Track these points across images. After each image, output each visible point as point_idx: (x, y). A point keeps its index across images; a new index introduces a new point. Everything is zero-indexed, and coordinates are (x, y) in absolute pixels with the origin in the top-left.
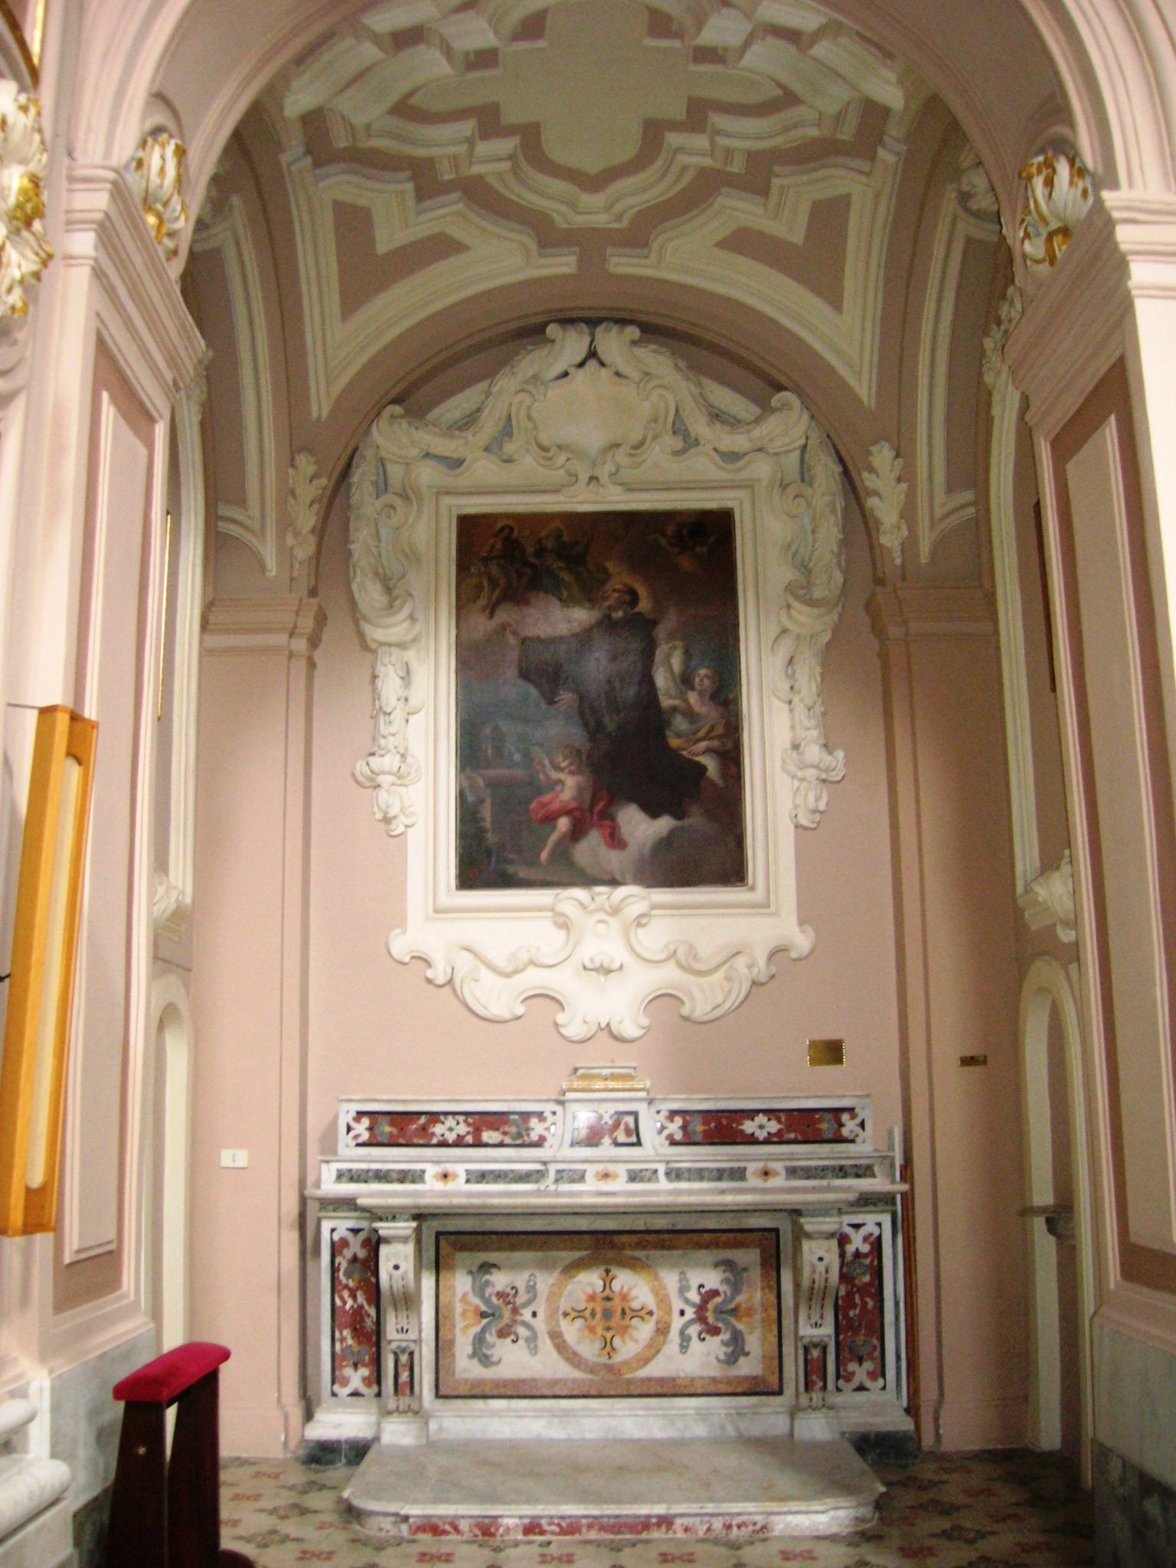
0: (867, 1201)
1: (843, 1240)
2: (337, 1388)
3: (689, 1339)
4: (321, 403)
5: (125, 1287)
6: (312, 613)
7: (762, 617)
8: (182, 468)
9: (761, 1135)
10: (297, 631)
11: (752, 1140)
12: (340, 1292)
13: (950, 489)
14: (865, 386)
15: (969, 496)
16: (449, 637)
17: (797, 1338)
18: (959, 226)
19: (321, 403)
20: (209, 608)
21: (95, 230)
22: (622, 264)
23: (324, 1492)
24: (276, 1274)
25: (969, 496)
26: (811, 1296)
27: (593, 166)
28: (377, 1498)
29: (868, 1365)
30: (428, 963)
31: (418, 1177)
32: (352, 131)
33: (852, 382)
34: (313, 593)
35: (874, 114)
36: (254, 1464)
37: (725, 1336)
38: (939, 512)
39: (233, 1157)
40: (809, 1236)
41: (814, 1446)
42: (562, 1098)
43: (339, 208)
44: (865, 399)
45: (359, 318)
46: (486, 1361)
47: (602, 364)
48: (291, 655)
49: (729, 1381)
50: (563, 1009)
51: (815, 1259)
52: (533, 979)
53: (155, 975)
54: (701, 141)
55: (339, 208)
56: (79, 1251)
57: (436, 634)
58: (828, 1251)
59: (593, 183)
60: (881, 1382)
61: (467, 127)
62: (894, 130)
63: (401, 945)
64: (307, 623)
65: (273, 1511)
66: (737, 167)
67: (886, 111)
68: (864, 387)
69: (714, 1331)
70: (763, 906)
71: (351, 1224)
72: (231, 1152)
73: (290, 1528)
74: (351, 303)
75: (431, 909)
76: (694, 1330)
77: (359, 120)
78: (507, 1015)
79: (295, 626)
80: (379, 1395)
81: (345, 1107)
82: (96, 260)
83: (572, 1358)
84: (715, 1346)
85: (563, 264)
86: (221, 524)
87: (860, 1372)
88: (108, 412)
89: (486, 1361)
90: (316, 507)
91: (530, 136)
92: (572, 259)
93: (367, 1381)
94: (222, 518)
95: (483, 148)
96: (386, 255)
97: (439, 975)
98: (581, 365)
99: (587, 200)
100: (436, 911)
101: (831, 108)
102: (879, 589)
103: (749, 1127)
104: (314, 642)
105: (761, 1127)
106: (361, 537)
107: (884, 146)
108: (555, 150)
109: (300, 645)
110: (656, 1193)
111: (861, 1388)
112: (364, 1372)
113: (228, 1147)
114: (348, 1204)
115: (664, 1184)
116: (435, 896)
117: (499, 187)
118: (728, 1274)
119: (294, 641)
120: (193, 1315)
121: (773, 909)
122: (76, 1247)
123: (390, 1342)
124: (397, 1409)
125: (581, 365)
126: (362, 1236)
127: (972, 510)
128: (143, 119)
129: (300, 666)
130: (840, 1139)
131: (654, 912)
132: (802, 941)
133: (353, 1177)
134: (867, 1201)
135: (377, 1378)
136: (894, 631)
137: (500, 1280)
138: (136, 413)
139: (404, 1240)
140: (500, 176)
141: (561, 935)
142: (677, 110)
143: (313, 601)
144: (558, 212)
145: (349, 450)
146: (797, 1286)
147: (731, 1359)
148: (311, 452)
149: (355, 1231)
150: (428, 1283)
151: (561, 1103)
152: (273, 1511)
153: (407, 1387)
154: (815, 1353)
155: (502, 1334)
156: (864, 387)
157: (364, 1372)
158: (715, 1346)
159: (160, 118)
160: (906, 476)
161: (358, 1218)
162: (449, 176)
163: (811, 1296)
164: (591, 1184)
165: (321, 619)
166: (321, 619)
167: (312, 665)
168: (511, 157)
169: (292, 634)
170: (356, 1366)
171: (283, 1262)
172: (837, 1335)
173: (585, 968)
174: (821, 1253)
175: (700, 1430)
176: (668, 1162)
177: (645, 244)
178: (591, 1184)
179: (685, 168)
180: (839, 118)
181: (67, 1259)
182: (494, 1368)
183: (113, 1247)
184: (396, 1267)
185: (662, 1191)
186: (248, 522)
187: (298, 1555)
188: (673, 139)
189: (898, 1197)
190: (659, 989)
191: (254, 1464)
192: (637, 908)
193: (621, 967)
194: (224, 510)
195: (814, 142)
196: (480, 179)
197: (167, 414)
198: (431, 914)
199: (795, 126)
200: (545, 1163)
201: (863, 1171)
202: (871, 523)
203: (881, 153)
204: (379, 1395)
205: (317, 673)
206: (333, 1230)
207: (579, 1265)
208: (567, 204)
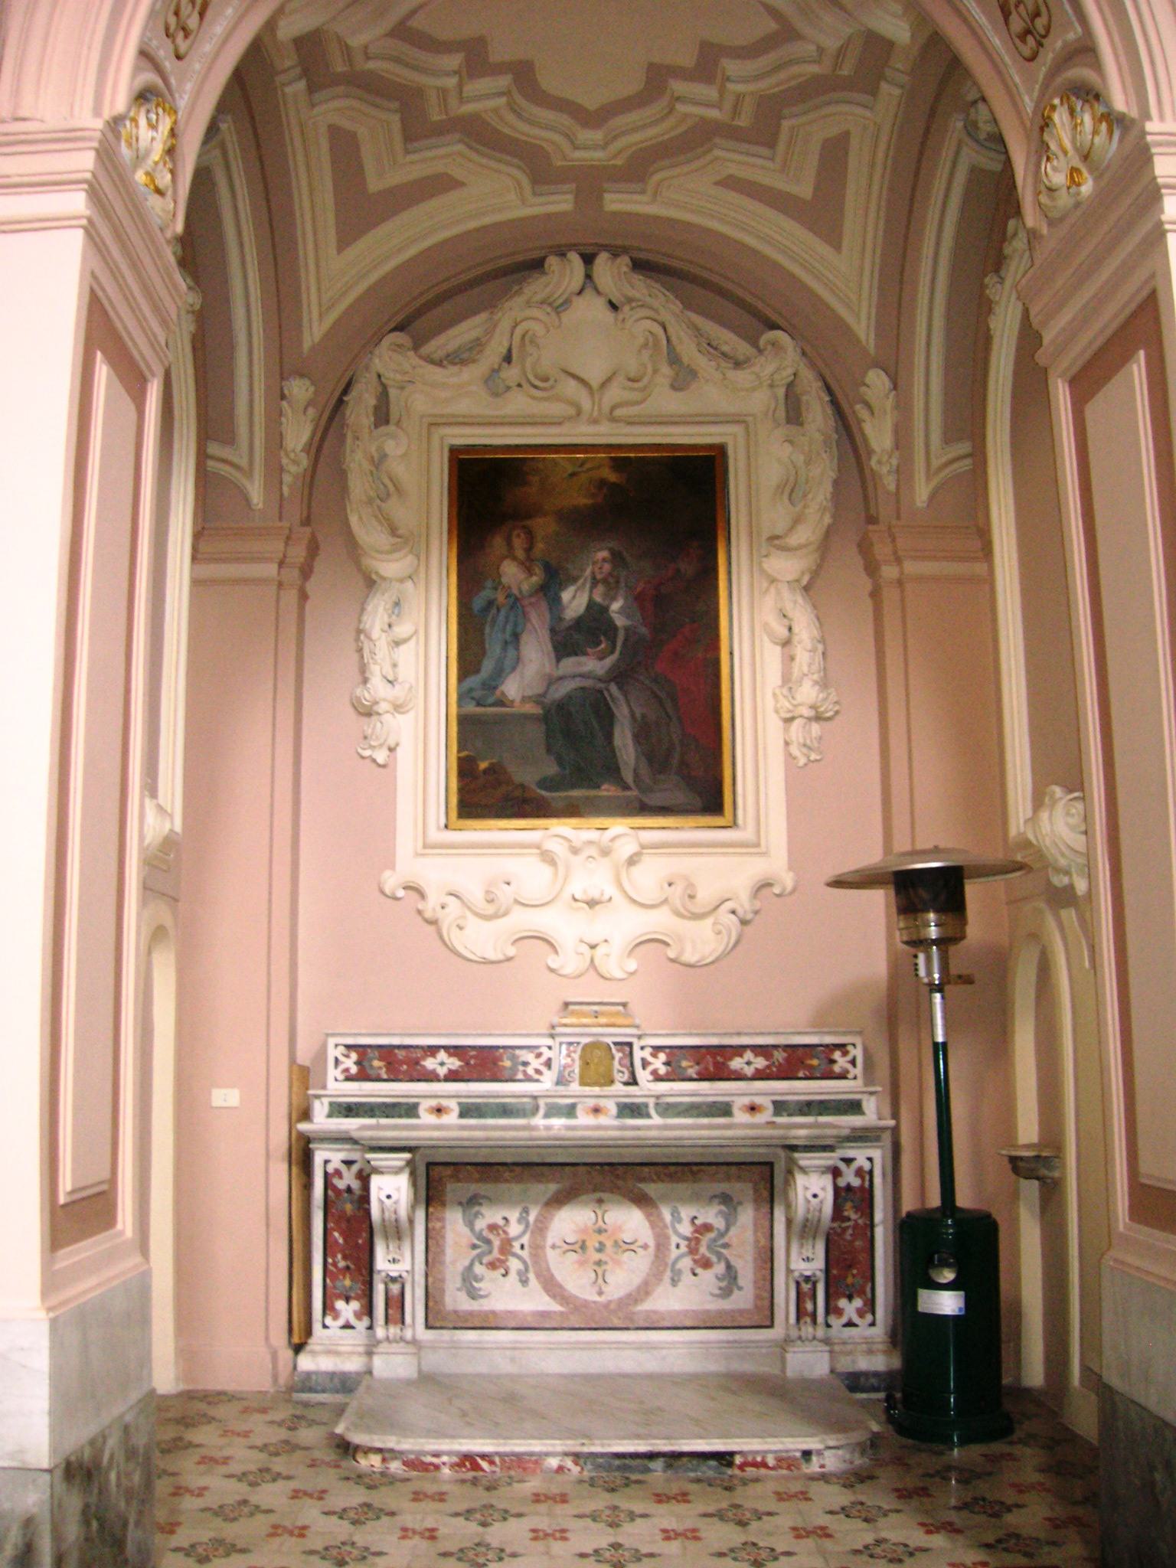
0: (861, 1136)
1: (836, 1173)
2: (328, 1320)
3: (680, 1272)
4: (314, 329)
5: (119, 1226)
6: (305, 542)
7: (756, 593)
8: (176, 412)
9: (749, 1071)
10: (288, 560)
11: (739, 1077)
12: (334, 1256)
13: (948, 440)
14: (864, 322)
15: (964, 447)
16: (440, 606)
17: (789, 1271)
18: (965, 150)
19: (314, 329)
20: (198, 536)
21: (86, 191)
22: (616, 202)
23: (315, 1427)
24: (263, 1209)
25: (964, 447)
26: (806, 1230)
27: (591, 101)
28: (369, 1430)
29: (858, 1303)
30: (422, 895)
31: (410, 1110)
32: (347, 51)
33: (849, 319)
34: (307, 521)
35: (877, 47)
36: (243, 1399)
37: (720, 1268)
38: (936, 463)
39: (226, 1097)
40: (803, 1170)
41: (807, 1385)
42: (553, 1032)
43: (334, 131)
44: (862, 336)
45: (351, 252)
46: (473, 1294)
47: (598, 292)
48: (917, 926)
49: (720, 1313)
50: (556, 952)
51: (809, 1196)
52: (522, 920)
53: (143, 903)
54: (710, 92)
55: (334, 131)
56: (73, 1192)
57: (427, 547)
58: (823, 1189)
59: (589, 118)
60: (869, 1317)
61: (454, 61)
62: (899, 63)
63: (391, 881)
64: (298, 553)
65: (263, 1448)
66: (743, 121)
67: (890, 44)
68: (863, 327)
69: (706, 1264)
70: (754, 846)
71: (342, 1156)
72: (223, 1091)
73: (279, 1465)
74: (346, 239)
75: (420, 844)
76: (686, 1263)
77: (356, 42)
78: (501, 957)
79: (285, 556)
80: (370, 1328)
81: (332, 1041)
82: (90, 221)
83: (551, 1286)
84: (709, 1278)
85: (561, 202)
86: (210, 463)
87: (850, 1308)
88: (102, 372)
89: (473, 1294)
90: (311, 411)
91: (523, 74)
92: (570, 197)
93: (358, 1316)
94: (212, 458)
95: (474, 87)
96: (380, 193)
97: (430, 907)
98: (580, 293)
99: (586, 135)
100: (425, 846)
101: (832, 44)
102: (871, 527)
103: (736, 1064)
104: (306, 572)
105: (748, 1063)
106: (357, 459)
107: (886, 80)
108: (549, 82)
109: (292, 575)
110: (649, 1128)
111: (850, 1324)
112: (355, 1305)
113: (219, 1087)
114: (346, 1139)
115: (656, 1120)
116: (424, 833)
117: (495, 122)
118: (723, 1208)
119: (284, 571)
120: (187, 1355)
121: (763, 849)
122: (69, 1188)
123: (379, 1272)
124: (387, 1339)
125: (580, 293)
126: (355, 1168)
127: (968, 461)
128: (134, 75)
129: (290, 597)
130: (829, 1076)
131: (645, 851)
132: (788, 880)
133: (350, 1110)
134: (861, 1136)
135: (369, 1310)
136: (889, 572)
137: (491, 1215)
138: (132, 379)
139: (398, 1171)
140: (496, 110)
141: (546, 871)
142: (686, 58)
143: (308, 530)
144: (553, 143)
145: (345, 381)
146: (789, 1222)
147: (726, 1292)
148: (302, 375)
149: (348, 1163)
150: (420, 1215)
151: (552, 1036)
152: (263, 1448)
153: (396, 1306)
154: (806, 1287)
155: (492, 1266)
156: (863, 327)
157: (355, 1305)
158: (709, 1278)
159: (149, 77)
160: (903, 407)
161: (348, 1150)
162: (436, 116)
163: (806, 1230)
164: (584, 1119)
165: (313, 549)
166: (313, 549)
167: (304, 596)
168: (507, 93)
169: (281, 564)
170: (347, 1300)
171: (272, 1197)
172: (827, 1271)
173: (575, 900)
174: (815, 1190)
175: (691, 1366)
176: (658, 1097)
177: (642, 179)
178: (584, 1119)
179: (686, 116)
180: (841, 53)
181: (62, 1199)
182: (482, 1301)
183: (105, 1187)
184: (389, 1197)
185: (654, 1127)
186: (235, 460)
187: (290, 1494)
188: (678, 87)
189: (980, 568)
190: (655, 932)
191: (243, 1399)
192: (627, 847)
193: (611, 899)
194: (213, 449)
195: (816, 78)
196: (475, 119)
197: (160, 372)
198: (420, 850)
199: (791, 63)
200: (535, 1098)
201: (854, 1107)
202: (862, 451)
203: (884, 86)
204: (370, 1328)
205: (308, 606)
206: (326, 1162)
207: (559, 1200)
208: (567, 136)
